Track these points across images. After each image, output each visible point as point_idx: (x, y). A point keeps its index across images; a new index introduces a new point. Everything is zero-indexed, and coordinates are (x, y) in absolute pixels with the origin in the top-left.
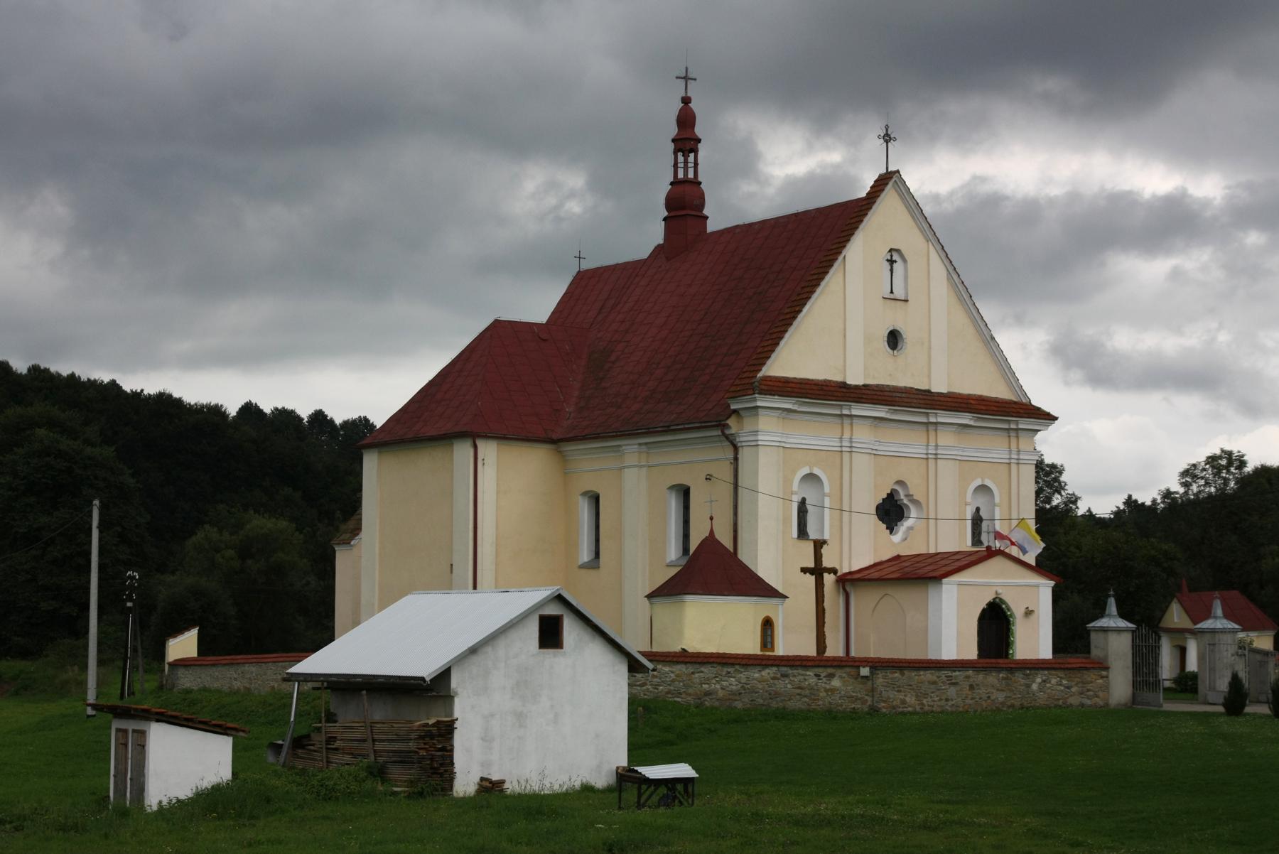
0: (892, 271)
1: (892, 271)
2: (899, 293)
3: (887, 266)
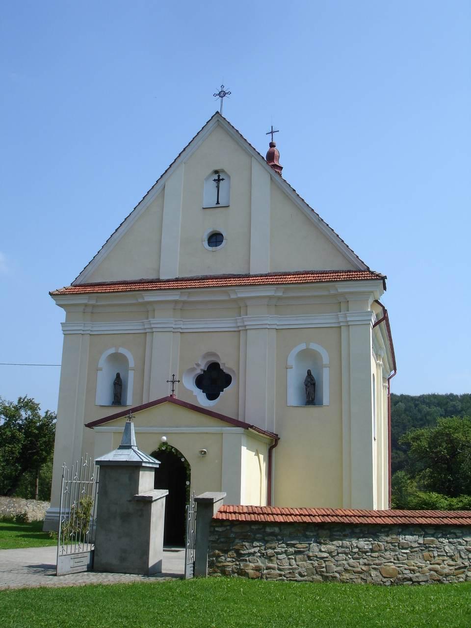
0: (218, 187)
1: (218, 187)
2: (222, 202)
3: (215, 184)
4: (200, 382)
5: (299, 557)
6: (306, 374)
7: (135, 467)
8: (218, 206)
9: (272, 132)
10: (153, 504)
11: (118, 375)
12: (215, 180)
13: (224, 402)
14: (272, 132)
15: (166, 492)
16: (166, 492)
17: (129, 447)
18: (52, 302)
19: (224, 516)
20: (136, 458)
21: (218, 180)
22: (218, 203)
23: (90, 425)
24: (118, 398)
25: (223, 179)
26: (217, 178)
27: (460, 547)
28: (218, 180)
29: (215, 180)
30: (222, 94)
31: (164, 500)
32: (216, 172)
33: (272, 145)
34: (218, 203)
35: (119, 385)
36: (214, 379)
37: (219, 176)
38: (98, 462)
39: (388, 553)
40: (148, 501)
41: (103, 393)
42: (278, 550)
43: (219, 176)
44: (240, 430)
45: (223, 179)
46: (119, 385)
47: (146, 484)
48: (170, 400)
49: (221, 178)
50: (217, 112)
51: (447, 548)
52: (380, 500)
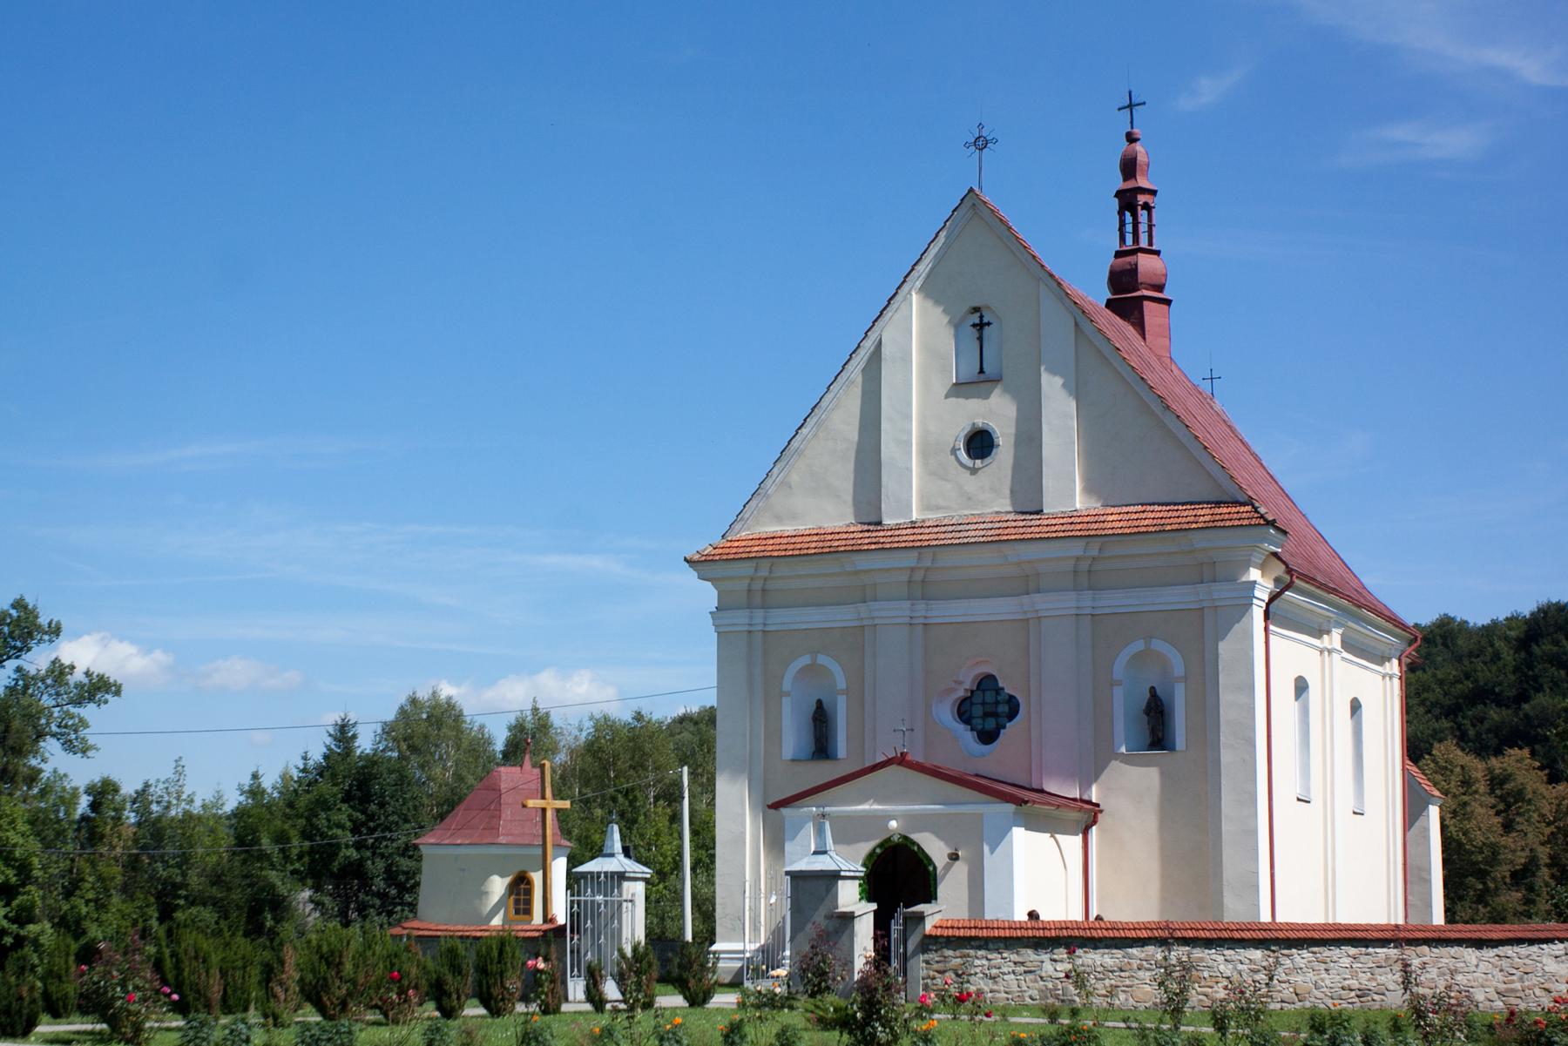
0: (980, 339)
1: (980, 339)
3: (974, 333)
4: (964, 712)
5: (1030, 977)
6: (1148, 695)
7: (834, 877)
8: (982, 377)
9: (1131, 106)
10: (856, 921)
11: (819, 703)
12: (974, 325)
13: (997, 759)
14: (1131, 106)
15: (874, 906)
16: (874, 906)
17: (825, 852)
18: (692, 575)
19: (939, 932)
20: (833, 867)
21: (981, 326)
22: (982, 371)
23: (770, 807)
24: (822, 748)
25: (989, 324)
26: (977, 321)
27: (1240, 967)
28: (981, 326)
29: (974, 325)
30: (981, 143)
31: (871, 916)
32: (976, 310)
33: (1131, 139)
34: (982, 371)
35: (821, 719)
36: (988, 709)
37: (981, 317)
38: (787, 873)
39: (1141, 973)
40: (849, 918)
41: (793, 737)
42: (1005, 970)
43: (981, 317)
44: (1011, 807)
45: (989, 324)
46: (821, 719)
47: (849, 896)
48: (901, 760)
49: (985, 320)
50: (971, 190)
51: (1222, 968)
52: (1438, 918)
